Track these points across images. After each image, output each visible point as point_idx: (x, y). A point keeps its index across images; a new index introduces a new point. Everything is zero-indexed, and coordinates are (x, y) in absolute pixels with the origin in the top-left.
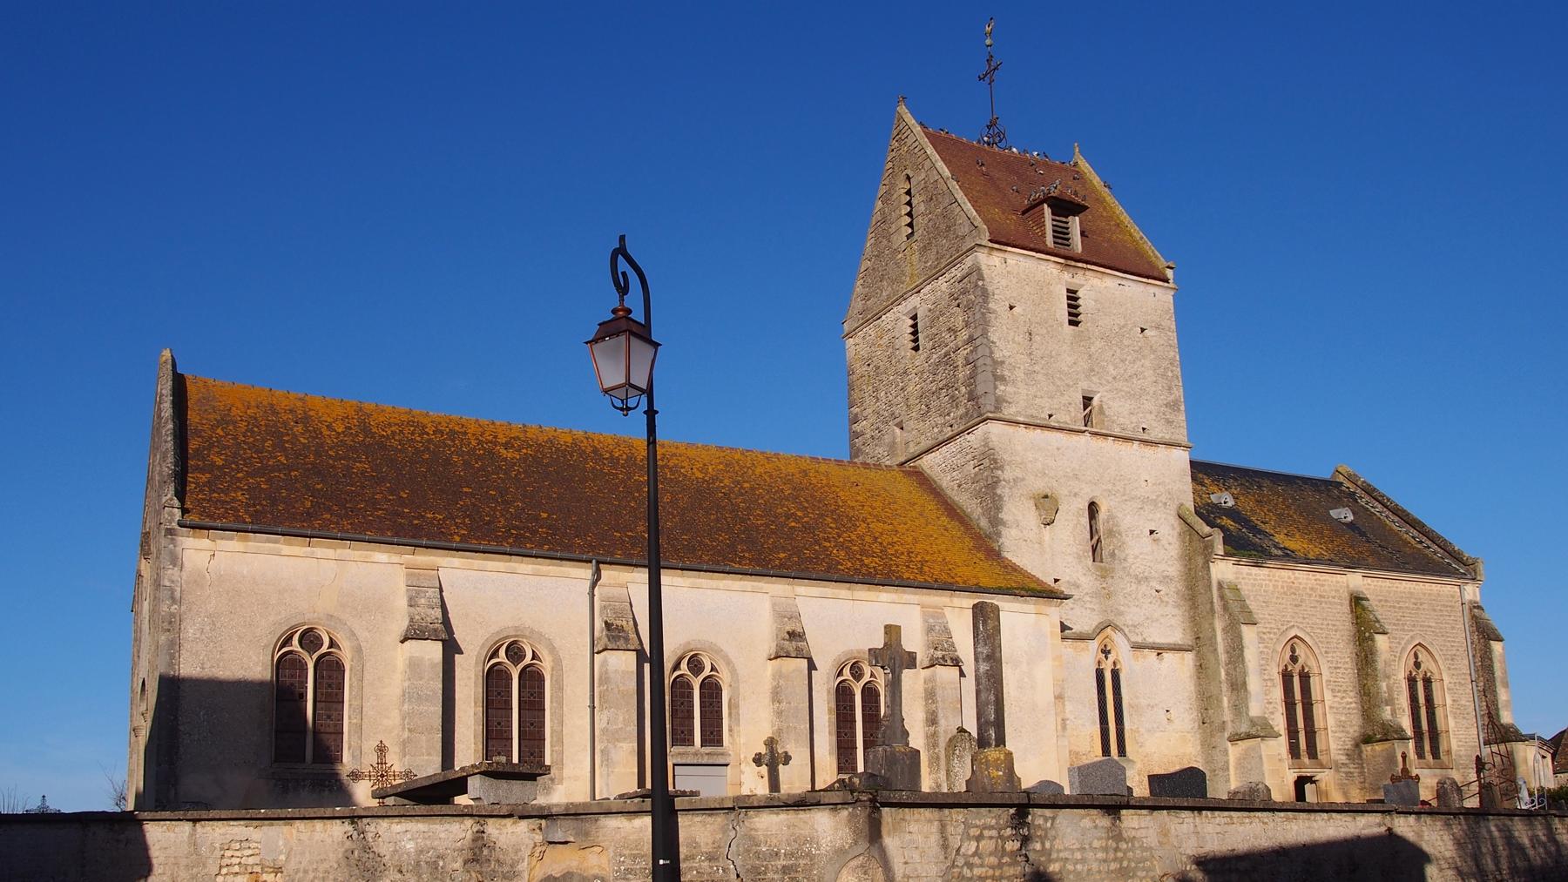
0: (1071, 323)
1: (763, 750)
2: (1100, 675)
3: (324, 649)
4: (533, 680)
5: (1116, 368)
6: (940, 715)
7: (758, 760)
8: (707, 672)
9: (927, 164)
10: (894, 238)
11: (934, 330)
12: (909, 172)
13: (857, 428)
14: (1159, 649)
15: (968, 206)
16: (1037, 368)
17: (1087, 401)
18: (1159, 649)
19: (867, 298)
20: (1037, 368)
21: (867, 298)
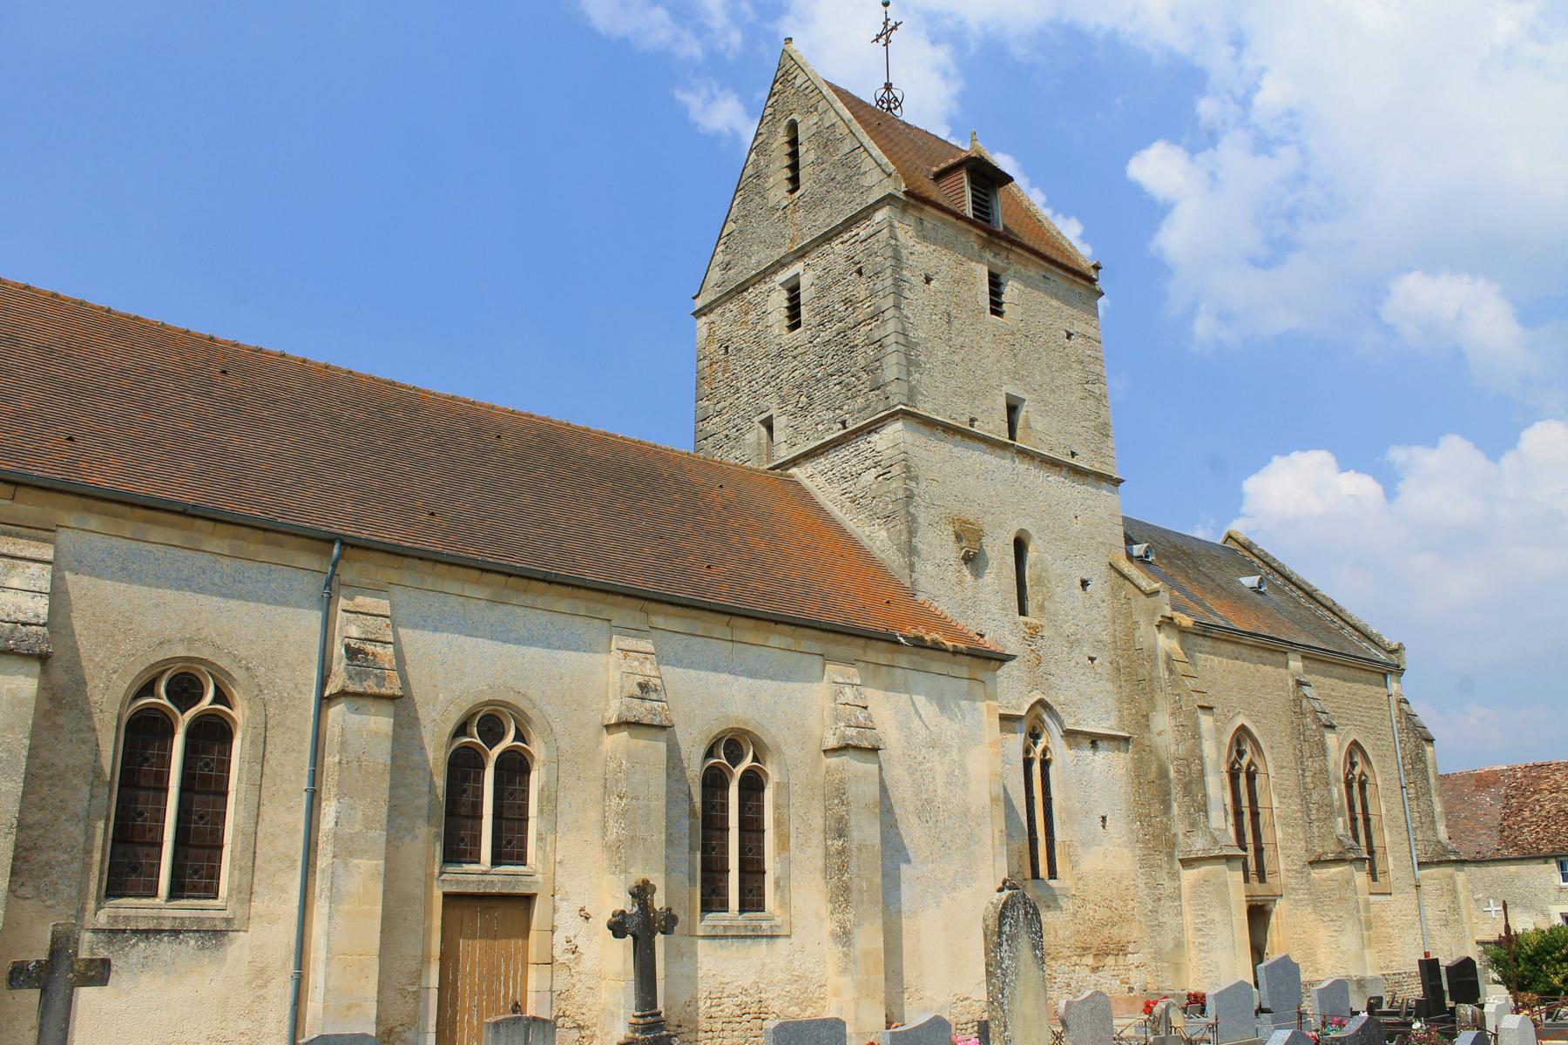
0: (994, 312)
1: (630, 907)
2: (1028, 763)
3: (206, 703)
4: (212, 735)
5: (1042, 374)
6: (852, 823)
7: (618, 927)
8: (508, 741)
9: (822, 106)
10: (771, 194)
11: (824, 302)
12: (795, 116)
13: (709, 427)
14: (1095, 740)
15: (876, 151)
16: (956, 358)
17: (1012, 409)
18: (1095, 740)
19: (727, 267)
20: (956, 358)
21: (727, 267)
